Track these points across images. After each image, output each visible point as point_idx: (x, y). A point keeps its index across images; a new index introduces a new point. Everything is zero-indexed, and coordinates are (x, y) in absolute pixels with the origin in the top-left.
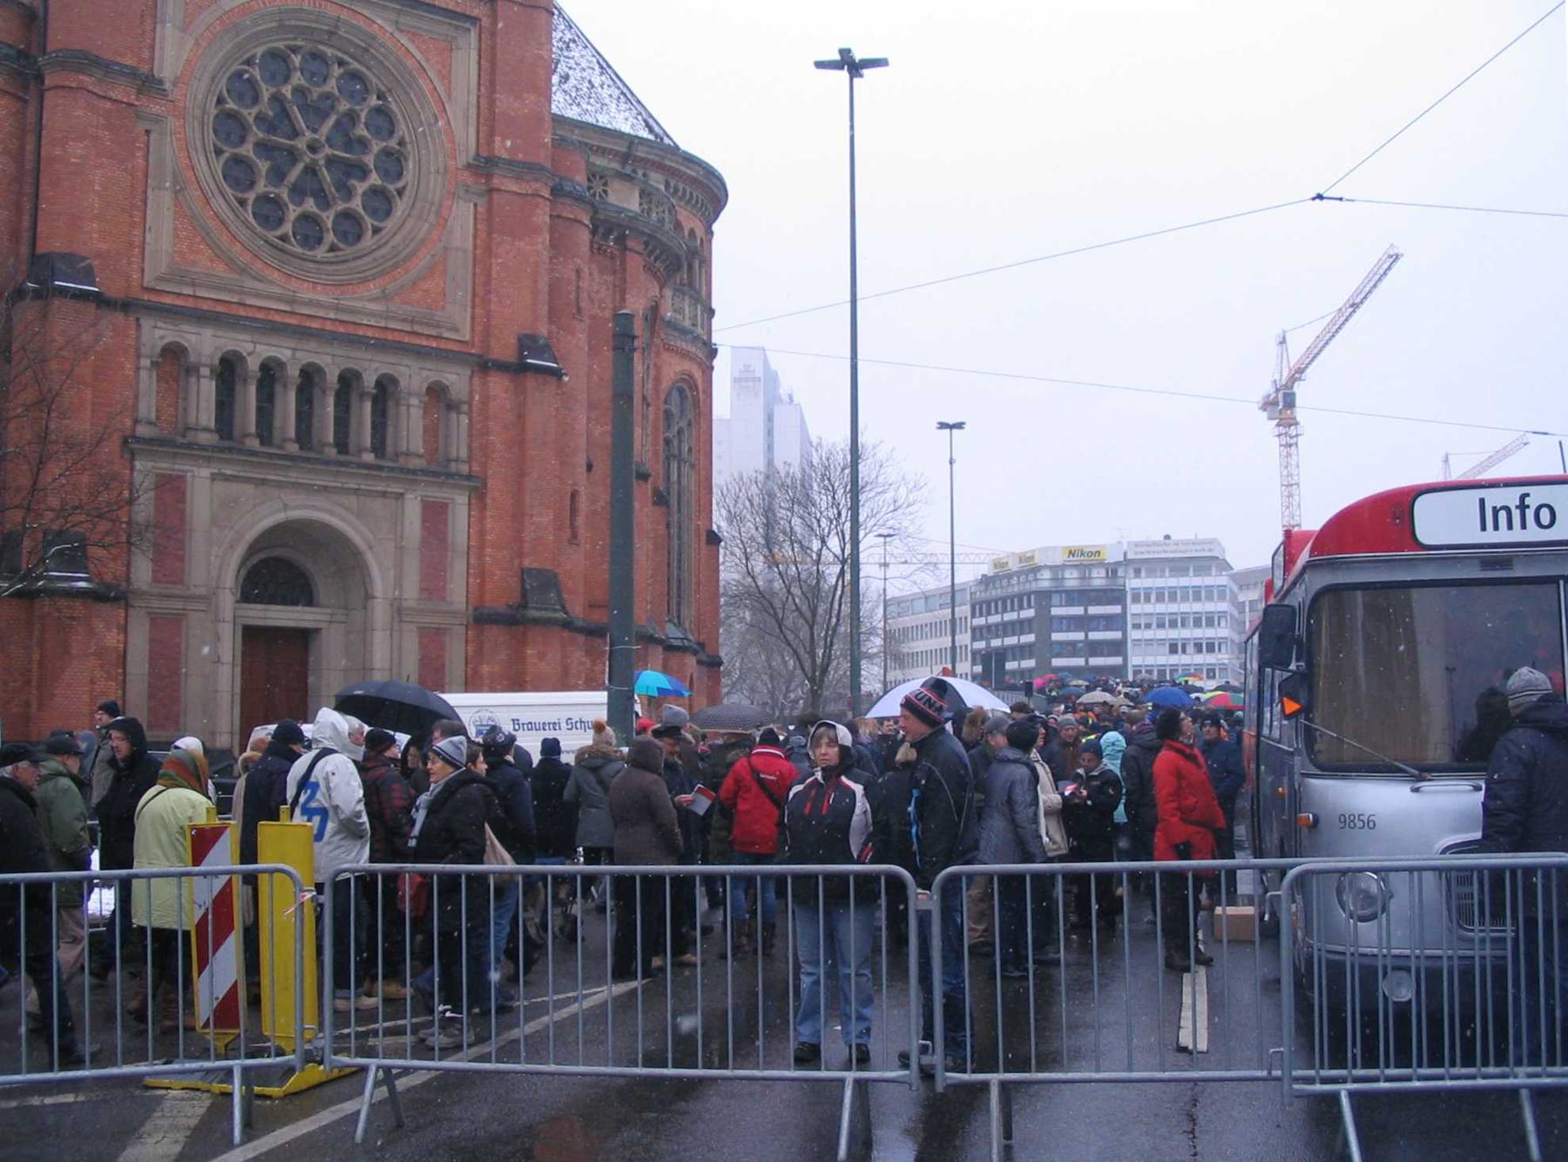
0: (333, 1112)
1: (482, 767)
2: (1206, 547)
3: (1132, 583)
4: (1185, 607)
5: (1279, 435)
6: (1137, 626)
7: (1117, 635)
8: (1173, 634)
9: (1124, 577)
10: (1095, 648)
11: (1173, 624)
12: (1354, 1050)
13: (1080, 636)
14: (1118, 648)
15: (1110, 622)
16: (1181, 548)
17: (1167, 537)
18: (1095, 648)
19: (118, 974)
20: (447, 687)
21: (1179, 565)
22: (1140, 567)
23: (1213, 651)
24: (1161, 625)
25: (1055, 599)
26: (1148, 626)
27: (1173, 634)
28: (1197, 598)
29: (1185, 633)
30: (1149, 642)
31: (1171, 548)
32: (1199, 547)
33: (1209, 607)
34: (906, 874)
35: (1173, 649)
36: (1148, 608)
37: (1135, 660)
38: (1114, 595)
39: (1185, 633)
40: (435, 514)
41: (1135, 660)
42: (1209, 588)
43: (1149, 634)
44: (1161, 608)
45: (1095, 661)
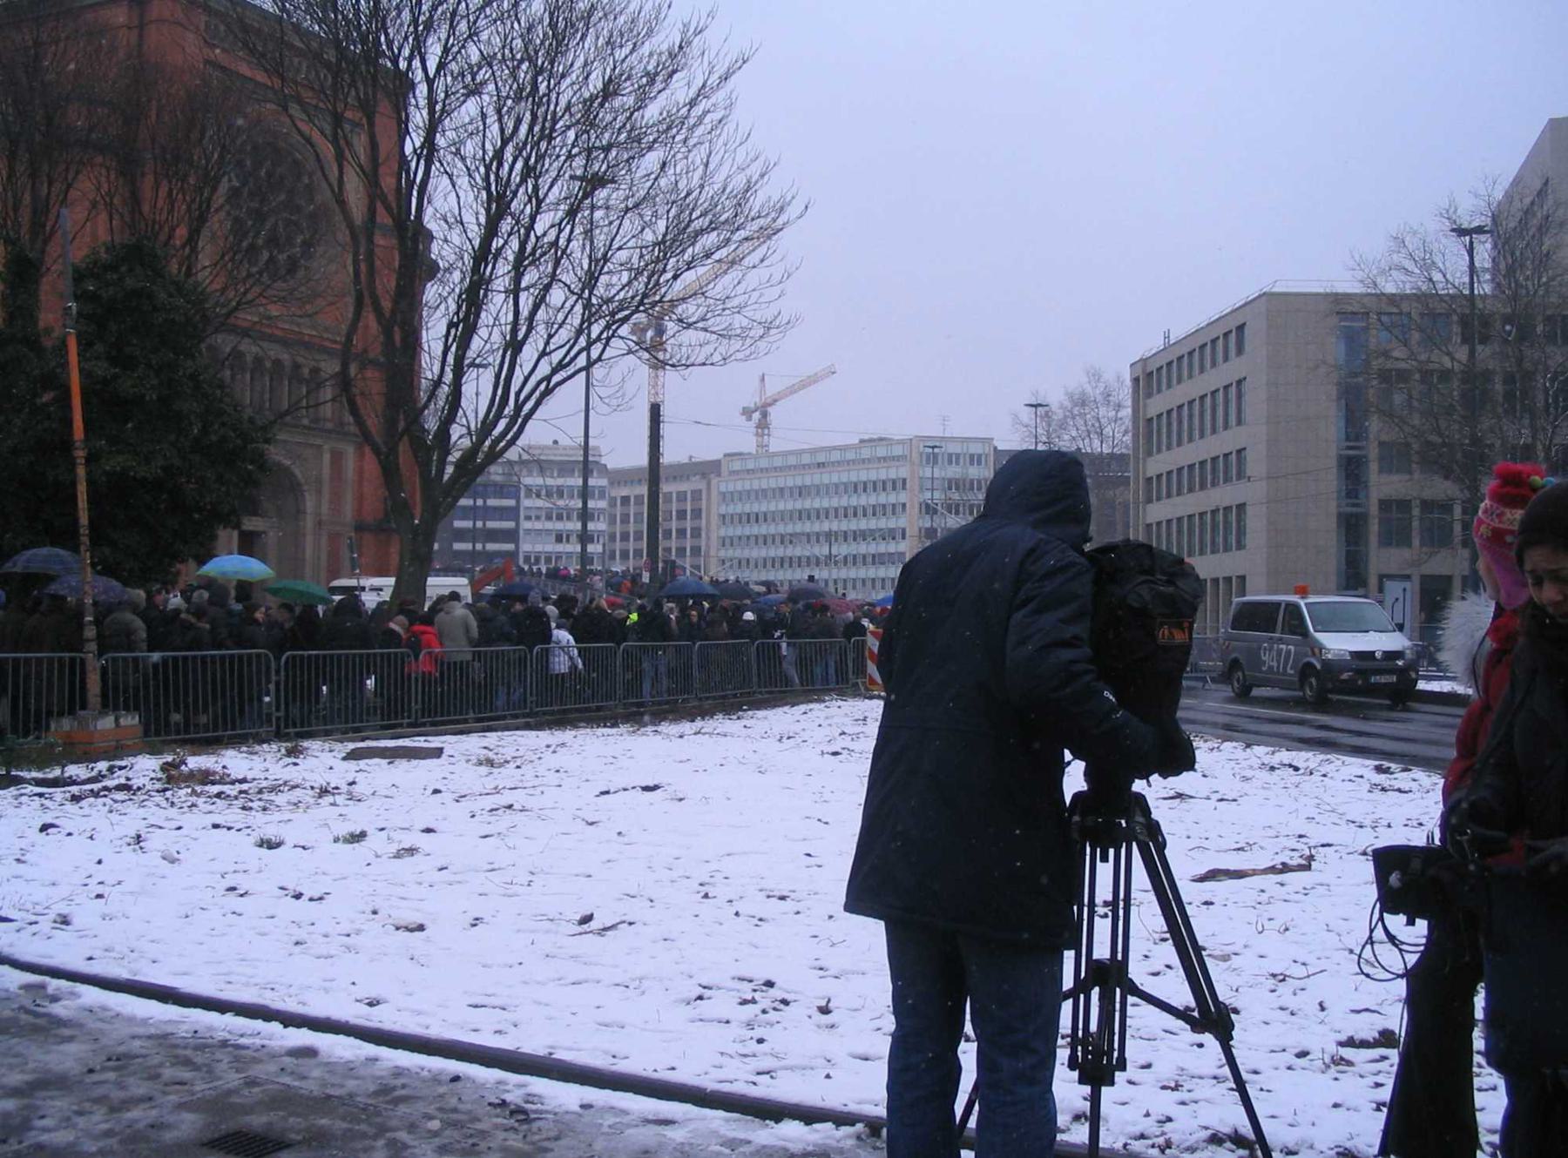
0: (817, 1131)
1: (99, 568)
3: (532, 480)
6: (528, 518)
7: (510, 525)
8: (559, 526)
10: (494, 536)
14: (512, 536)
15: (502, 513)
17: (556, 442)
18: (494, 536)
19: (131, 684)
24: (549, 518)
26: (538, 518)
27: (559, 526)
31: (561, 452)
34: (271, 655)
35: (559, 539)
37: (526, 547)
40: (337, 458)
41: (526, 547)
43: (538, 525)
45: (491, 547)
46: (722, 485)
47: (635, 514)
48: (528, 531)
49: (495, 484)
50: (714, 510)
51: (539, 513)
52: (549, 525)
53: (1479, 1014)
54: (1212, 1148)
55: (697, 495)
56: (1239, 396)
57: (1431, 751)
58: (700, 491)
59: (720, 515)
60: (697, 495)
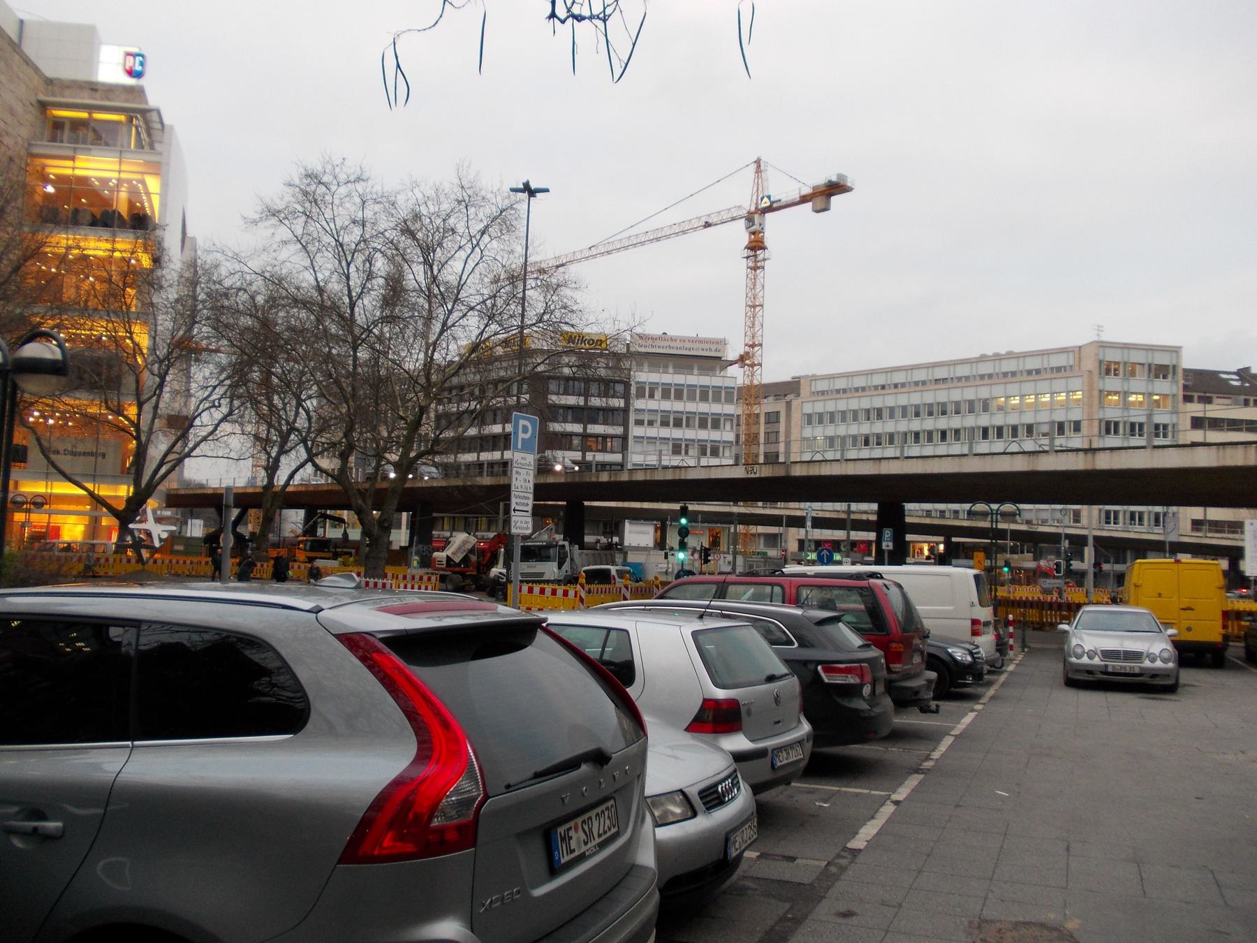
2: (713, 347)
3: (644, 376)
4: (691, 407)
5: (747, 258)
6: (639, 423)
8: (677, 433)
9: (630, 370)
11: (678, 424)
12: (704, 801)
13: (577, 428)
15: (607, 415)
16: (688, 345)
20: (536, 518)
21: (684, 361)
22: (659, 360)
23: (1159, 437)
24: (665, 424)
25: (553, 386)
26: (651, 423)
27: (677, 433)
28: (704, 398)
29: (690, 434)
30: (652, 440)
32: (707, 346)
33: (716, 408)
35: (676, 449)
36: (652, 405)
38: (617, 384)
39: (690, 434)
42: (692, 388)
43: (652, 432)
44: (666, 405)
46: (805, 405)
47: (767, 434)
48: (639, 439)
49: (600, 380)
50: (795, 434)
51: (652, 418)
52: (665, 432)
53: (838, 788)
54: (763, 861)
55: (772, 418)
56: (1080, 353)
57: (80, 508)
58: (778, 413)
59: (826, 438)
60: (772, 418)
